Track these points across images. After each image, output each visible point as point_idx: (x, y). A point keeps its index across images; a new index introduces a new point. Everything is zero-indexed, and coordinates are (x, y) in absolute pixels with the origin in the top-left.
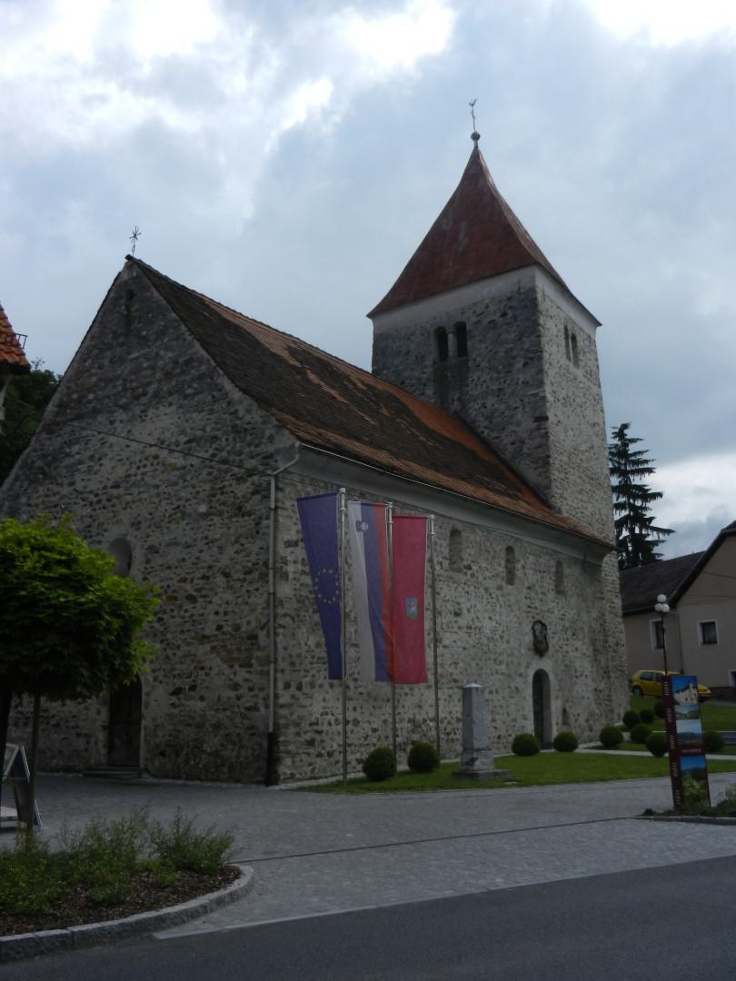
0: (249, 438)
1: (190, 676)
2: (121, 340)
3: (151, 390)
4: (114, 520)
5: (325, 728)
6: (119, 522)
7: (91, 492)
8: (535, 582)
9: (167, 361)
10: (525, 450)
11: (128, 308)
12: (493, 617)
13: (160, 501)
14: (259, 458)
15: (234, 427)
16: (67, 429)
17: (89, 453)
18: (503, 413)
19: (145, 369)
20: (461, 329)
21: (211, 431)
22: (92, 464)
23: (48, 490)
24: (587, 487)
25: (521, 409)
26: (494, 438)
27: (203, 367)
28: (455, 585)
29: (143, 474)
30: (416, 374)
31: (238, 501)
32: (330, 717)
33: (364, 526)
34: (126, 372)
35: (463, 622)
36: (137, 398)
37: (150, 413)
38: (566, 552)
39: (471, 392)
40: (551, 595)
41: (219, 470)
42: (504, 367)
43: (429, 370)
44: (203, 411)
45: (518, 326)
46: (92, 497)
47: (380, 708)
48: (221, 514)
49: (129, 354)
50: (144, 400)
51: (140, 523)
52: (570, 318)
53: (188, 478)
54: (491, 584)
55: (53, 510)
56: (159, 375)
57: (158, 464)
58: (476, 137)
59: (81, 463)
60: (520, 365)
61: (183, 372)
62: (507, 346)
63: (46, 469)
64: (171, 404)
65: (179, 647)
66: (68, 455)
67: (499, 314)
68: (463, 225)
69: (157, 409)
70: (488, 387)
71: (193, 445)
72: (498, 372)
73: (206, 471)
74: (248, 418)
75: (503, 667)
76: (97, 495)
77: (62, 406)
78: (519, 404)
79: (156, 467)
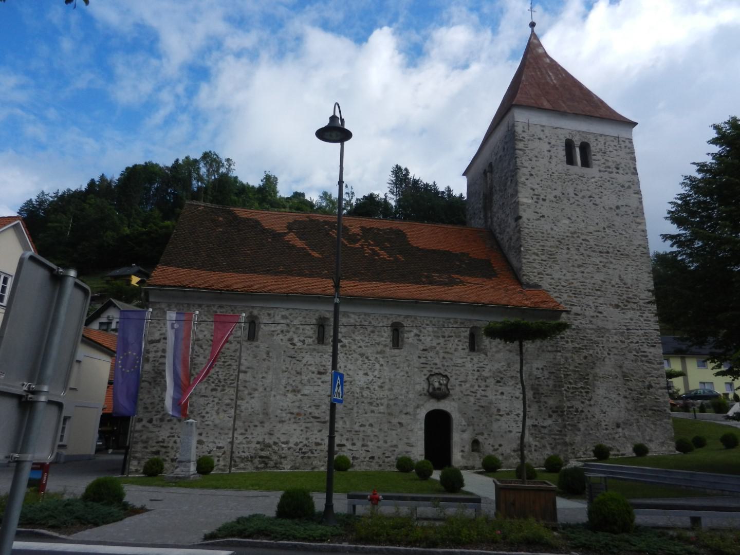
5: (170, 445)
12: (370, 373)
32: (176, 438)
52: (584, 132)
58: (533, 25)
75: (382, 409)
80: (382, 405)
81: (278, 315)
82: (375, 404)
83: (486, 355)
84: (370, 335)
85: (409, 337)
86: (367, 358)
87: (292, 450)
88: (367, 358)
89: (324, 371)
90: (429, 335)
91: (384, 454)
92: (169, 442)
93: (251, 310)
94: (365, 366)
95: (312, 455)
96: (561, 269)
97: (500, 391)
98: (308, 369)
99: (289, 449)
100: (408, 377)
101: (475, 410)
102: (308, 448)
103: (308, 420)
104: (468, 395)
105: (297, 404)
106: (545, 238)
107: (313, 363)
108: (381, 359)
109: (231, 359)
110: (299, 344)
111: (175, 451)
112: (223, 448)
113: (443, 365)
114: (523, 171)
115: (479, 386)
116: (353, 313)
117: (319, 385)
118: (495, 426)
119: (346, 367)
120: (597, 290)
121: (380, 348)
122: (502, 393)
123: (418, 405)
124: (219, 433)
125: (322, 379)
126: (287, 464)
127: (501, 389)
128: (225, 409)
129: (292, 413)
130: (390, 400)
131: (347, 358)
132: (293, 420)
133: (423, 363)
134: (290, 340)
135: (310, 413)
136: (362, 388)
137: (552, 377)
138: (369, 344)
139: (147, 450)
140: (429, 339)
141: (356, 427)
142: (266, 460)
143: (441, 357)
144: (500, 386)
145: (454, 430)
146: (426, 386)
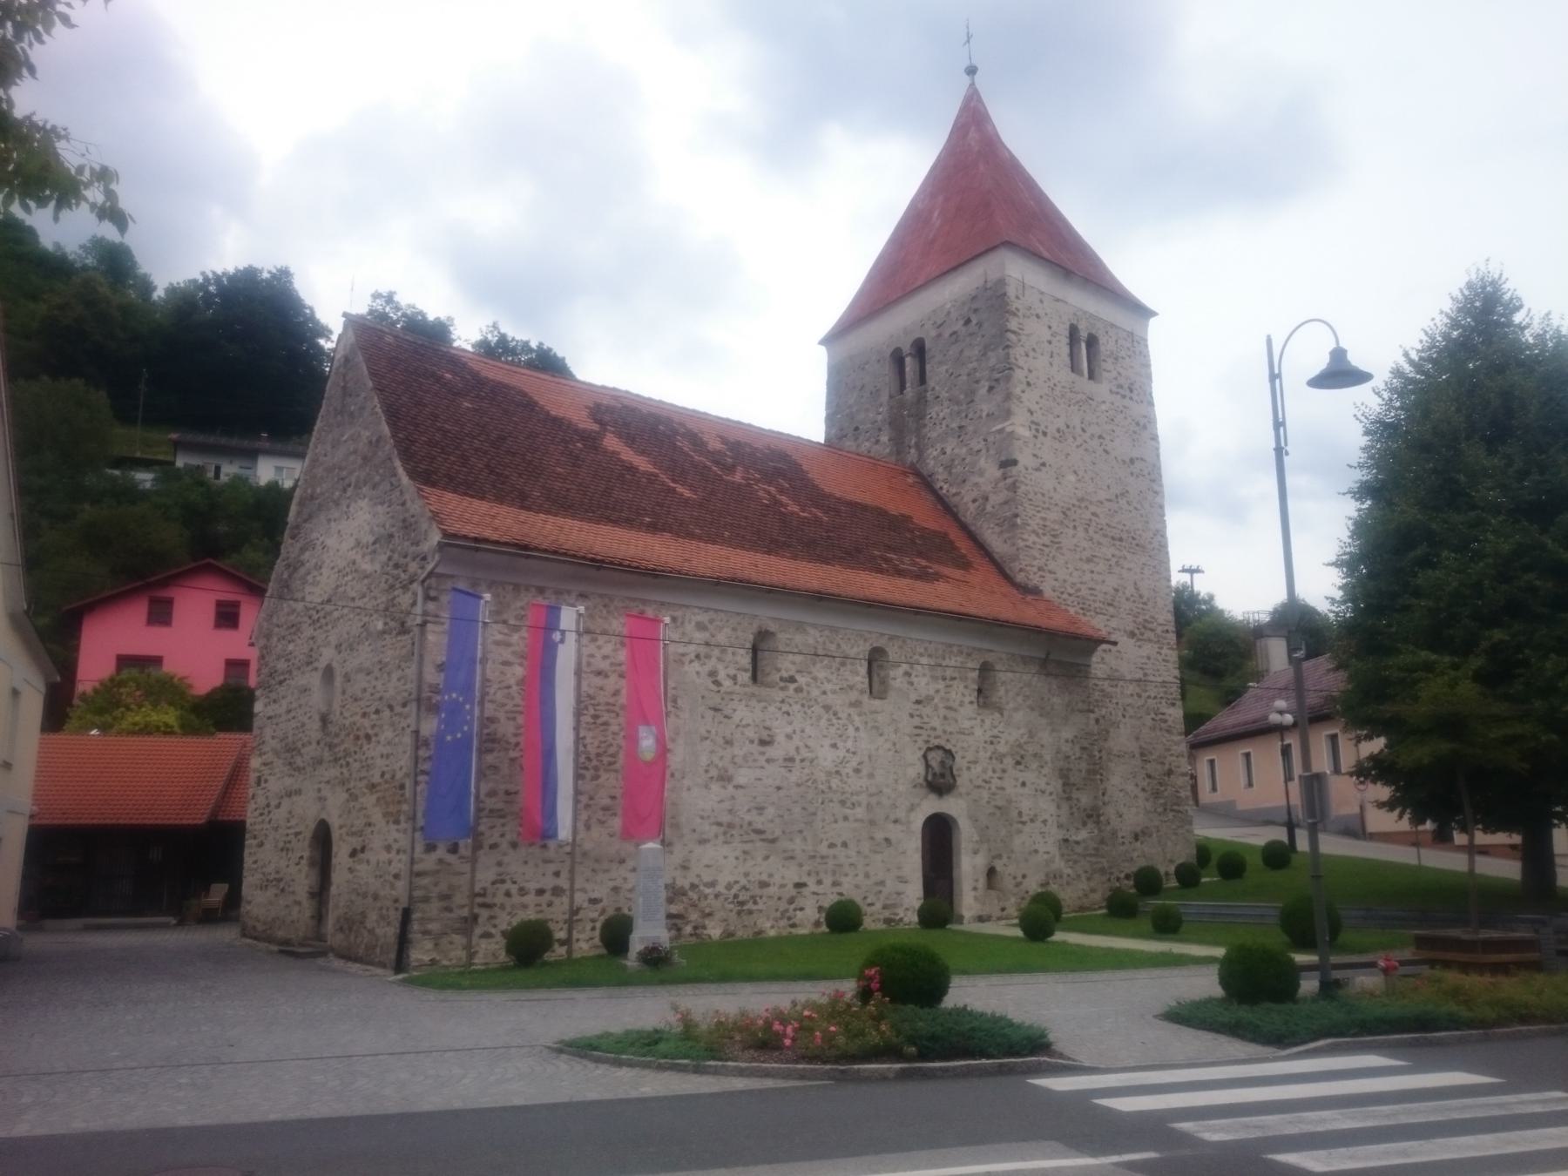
5: (500, 899)
10: (989, 508)
12: (840, 744)
14: (418, 559)
20: (920, 349)
24: (1108, 551)
25: (984, 451)
26: (954, 495)
33: (557, 636)
35: (775, 752)
38: (998, 652)
40: (969, 710)
45: (983, 336)
47: (607, 871)
54: (837, 701)
58: (972, 71)
60: (983, 391)
62: (971, 366)
67: (962, 322)
70: (947, 426)
71: (377, 546)
72: (958, 403)
75: (860, 812)
77: (301, 504)
78: (981, 445)
80: (860, 805)
81: (690, 622)
82: (849, 804)
83: (1002, 714)
84: (839, 669)
85: (896, 676)
86: (835, 714)
87: (722, 898)
88: (835, 714)
89: (768, 739)
90: (924, 675)
91: (865, 898)
92: (494, 895)
93: (641, 607)
94: (833, 730)
95: (755, 907)
96: (1067, 563)
97: (1021, 780)
98: (743, 734)
99: (717, 896)
100: (896, 751)
101: (990, 814)
102: (749, 894)
103: (746, 838)
104: (979, 787)
105: (727, 805)
106: (1047, 505)
107: (750, 721)
108: (856, 718)
109: (608, 711)
110: (727, 683)
111: (509, 914)
112: (601, 901)
113: (945, 732)
114: (1019, 375)
115: (994, 771)
116: (814, 626)
117: (762, 767)
118: (1017, 842)
119: (803, 731)
120: (1109, 605)
121: (854, 696)
122: (1024, 784)
123: (912, 805)
124: (593, 870)
125: (767, 756)
126: (714, 928)
127: (1022, 776)
128: (604, 819)
129: (719, 824)
130: (871, 795)
131: (805, 713)
132: (721, 838)
133: (916, 727)
134: (713, 674)
135: (750, 824)
136: (829, 774)
137: (1085, 756)
138: (837, 687)
139: (452, 915)
140: (924, 681)
141: (823, 849)
142: (678, 922)
143: (941, 716)
144: (1021, 771)
145: (963, 851)
146: (921, 769)
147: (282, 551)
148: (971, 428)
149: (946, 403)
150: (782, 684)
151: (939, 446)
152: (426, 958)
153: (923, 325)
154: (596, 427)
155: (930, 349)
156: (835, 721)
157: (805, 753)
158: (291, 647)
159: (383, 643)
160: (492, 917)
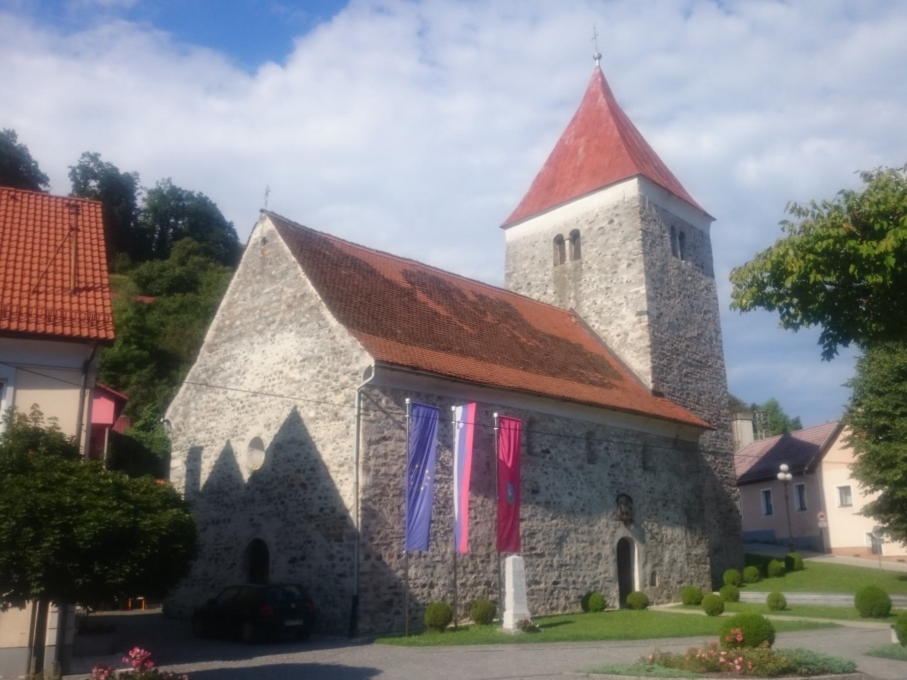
0: (343, 358)
1: (301, 549)
2: (258, 277)
3: (278, 318)
4: (253, 422)
6: (257, 423)
7: (238, 400)
8: (619, 460)
9: (289, 295)
10: (629, 341)
11: (263, 252)
12: (573, 493)
13: (284, 408)
14: (350, 374)
15: (333, 349)
16: (223, 349)
17: (236, 369)
18: (610, 309)
19: (274, 301)
20: (575, 236)
21: (318, 352)
22: (239, 377)
23: (209, 397)
26: (603, 331)
27: (312, 301)
28: (533, 467)
29: (273, 386)
30: (540, 276)
31: (335, 408)
34: (262, 303)
36: (269, 325)
37: (277, 337)
39: (584, 292)
40: (638, 471)
41: (323, 384)
42: (611, 268)
43: (550, 273)
44: (312, 336)
46: (239, 404)
48: (323, 418)
49: (264, 289)
50: (273, 327)
51: (270, 425)
53: (303, 389)
55: (212, 413)
56: (283, 307)
57: (283, 378)
59: (231, 376)
60: (624, 266)
61: (300, 304)
62: (614, 249)
63: (208, 380)
64: (291, 331)
65: (294, 525)
66: (223, 370)
67: (607, 222)
68: (583, 140)
69: (282, 333)
71: (306, 363)
72: (606, 273)
73: (314, 384)
74: (342, 342)
76: (242, 402)
78: (623, 300)
79: (281, 380)
83: (655, 474)
113: (626, 485)
115: (653, 510)
147: (198, 360)
148: (615, 289)
149: (596, 272)
150: (542, 454)
151: (591, 299)
152: (368, 628)
153: (578, 221)
154: (409, 286)
155: (584, 237)
156: (570, 478)
157: (556, 499)
158: (213, 424)
159: (316, 425)
160: (400, 602)
